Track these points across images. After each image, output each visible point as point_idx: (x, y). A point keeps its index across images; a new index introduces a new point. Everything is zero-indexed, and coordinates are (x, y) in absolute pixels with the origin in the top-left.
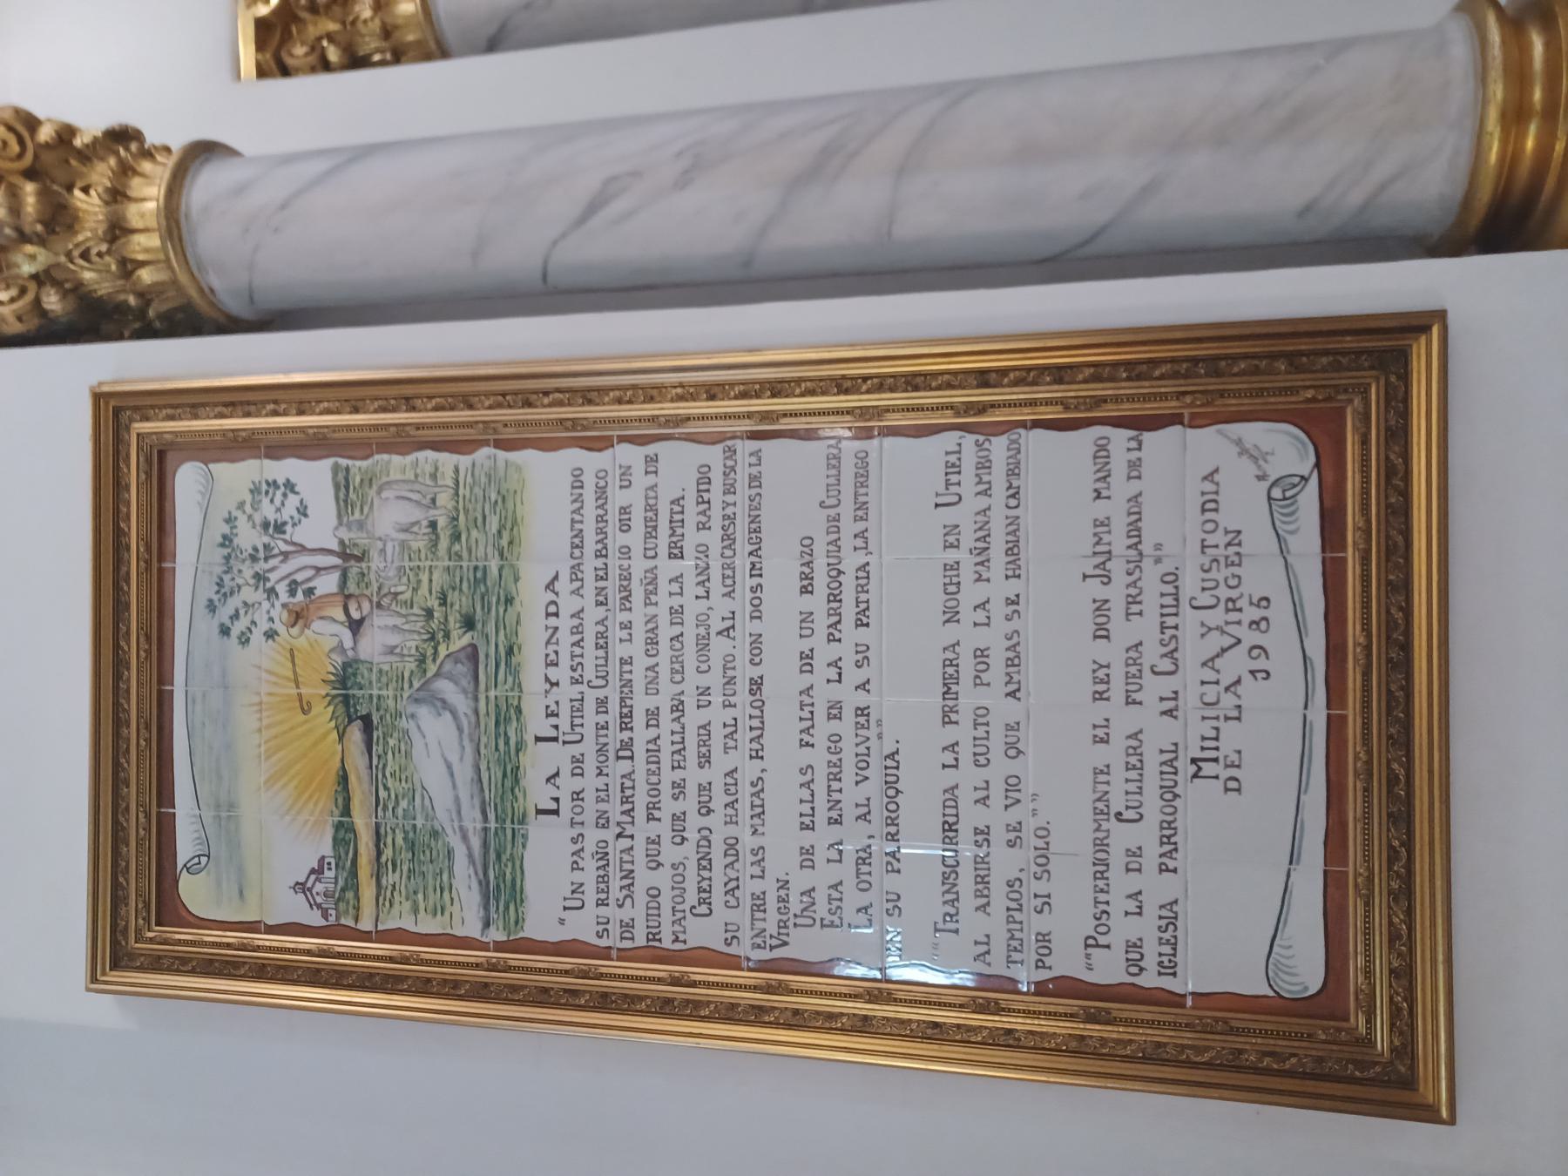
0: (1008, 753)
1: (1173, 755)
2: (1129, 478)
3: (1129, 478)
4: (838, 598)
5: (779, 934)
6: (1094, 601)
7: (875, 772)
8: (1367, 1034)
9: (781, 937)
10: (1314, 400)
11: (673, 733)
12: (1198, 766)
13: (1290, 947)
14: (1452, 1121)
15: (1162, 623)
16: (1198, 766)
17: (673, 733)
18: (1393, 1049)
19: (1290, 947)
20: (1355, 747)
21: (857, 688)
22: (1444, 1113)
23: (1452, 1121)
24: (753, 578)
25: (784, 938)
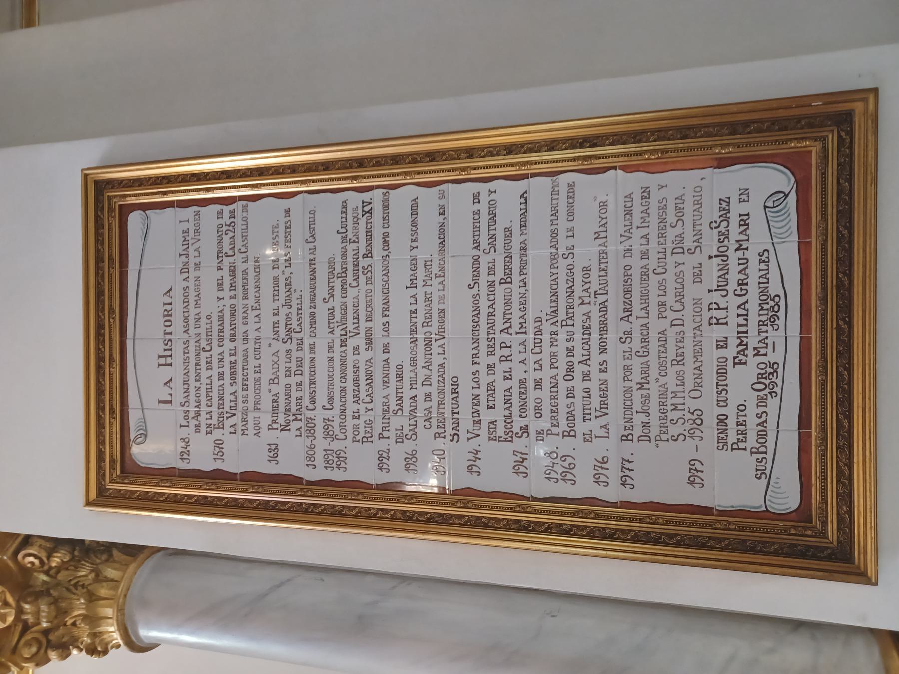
0: (574, 432)
1: (767, 271)
2: (218, 218)
3: (218, 218)
4: (493, 314)
5: (601, 408)
6: (606, 353)
7: (531, 405)
8: (822, 530)
9: (602, 410)
10: (649, 159)
11: (231, 401)
12: (740, 340)
13: (780, 488)
14: (876, 584)
15: (584, 417)
16: (740, 340)
17: (231, 401)
18: (839, 541)
19: (780, 488)
20: (827, 543)
21: (520, 362)
22: (873, 581)
23: (876, 584)
24: (232, 291)
25: (605, 411)
